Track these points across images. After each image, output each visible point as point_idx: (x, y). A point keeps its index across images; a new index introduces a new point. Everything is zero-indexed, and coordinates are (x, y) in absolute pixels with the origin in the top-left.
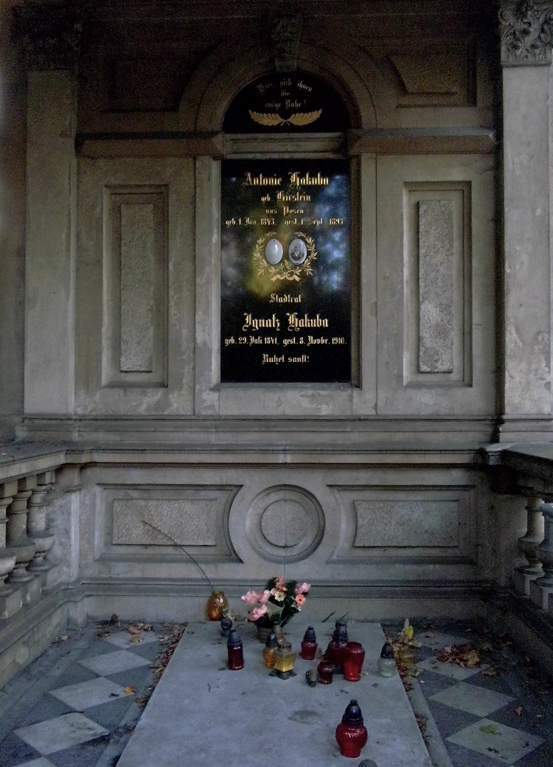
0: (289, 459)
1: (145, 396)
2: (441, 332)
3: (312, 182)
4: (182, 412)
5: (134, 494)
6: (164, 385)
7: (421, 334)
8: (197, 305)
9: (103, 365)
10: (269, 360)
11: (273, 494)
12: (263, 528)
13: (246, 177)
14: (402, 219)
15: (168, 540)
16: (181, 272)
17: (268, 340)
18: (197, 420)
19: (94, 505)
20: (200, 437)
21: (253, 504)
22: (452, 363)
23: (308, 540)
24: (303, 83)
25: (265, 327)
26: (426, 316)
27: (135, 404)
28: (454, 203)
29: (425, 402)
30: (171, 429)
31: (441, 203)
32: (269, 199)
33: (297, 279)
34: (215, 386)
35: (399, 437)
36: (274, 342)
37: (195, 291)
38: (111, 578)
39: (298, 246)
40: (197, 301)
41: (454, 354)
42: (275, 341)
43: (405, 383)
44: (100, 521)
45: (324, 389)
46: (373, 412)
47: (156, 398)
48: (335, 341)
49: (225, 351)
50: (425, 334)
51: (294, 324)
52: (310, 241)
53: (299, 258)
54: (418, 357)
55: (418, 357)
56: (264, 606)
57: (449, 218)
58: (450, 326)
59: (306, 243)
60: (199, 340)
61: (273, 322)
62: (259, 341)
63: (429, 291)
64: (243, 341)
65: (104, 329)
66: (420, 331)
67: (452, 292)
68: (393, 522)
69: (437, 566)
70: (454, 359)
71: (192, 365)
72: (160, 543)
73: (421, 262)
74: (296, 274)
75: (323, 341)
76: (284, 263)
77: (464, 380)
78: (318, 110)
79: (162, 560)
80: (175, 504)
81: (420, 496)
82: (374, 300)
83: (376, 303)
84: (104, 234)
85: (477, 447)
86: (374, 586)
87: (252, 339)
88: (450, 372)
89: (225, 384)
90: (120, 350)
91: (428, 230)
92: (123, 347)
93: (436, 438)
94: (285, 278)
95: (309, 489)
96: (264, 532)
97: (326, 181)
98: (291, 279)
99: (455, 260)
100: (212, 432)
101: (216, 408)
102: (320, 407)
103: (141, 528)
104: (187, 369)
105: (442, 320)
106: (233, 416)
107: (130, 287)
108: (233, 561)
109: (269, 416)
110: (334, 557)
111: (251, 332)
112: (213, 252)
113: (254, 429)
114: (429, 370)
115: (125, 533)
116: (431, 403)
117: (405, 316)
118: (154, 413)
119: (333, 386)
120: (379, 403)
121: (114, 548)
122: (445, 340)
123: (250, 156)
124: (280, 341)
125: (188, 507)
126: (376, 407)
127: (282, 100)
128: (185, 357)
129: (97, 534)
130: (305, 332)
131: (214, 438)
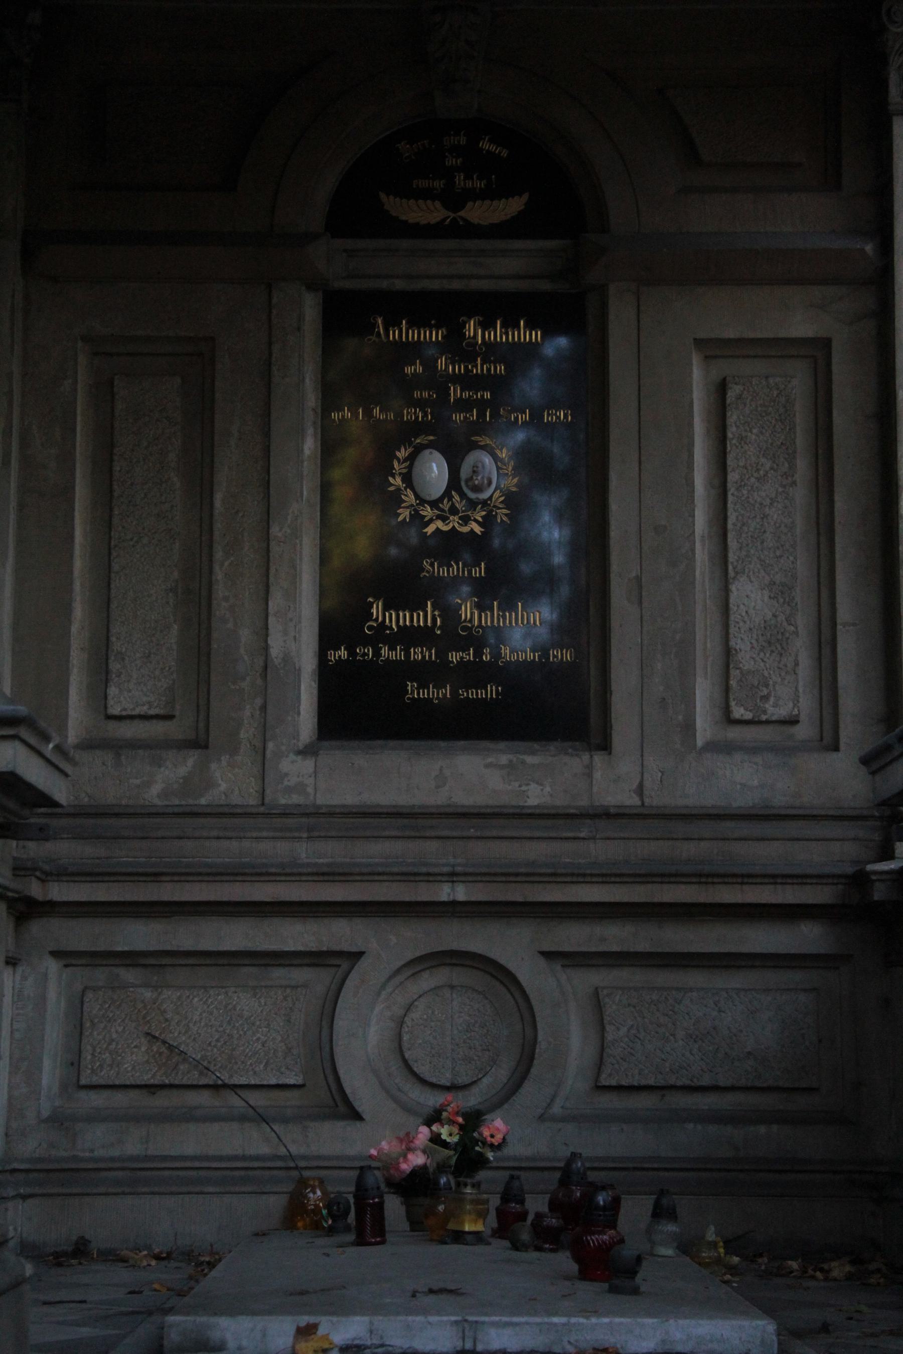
0: (461, 893)
1: (160, 767)
2: (774, 639)
3: (507, 338)
4: (235, 799)
5: (129, 975)
6: (198, 743)
7: (732, 643)
8: (271, 579)
9: (70, 702)
10: (418, 694)
11: (426, 975)
12: (405, 1045)
13: (375, 325)
14: (692, 416)
15: (201, 1073)
16: (237, 512)
17: (417, 654)
18: (267, 815)
19: (42, 998)
20: (279, 850)
21: (384, 994)
22: (796, 701)
23: (501, 1074)
24: (491, 141)
25: (412, 626)
26: (742, 606)
27: (138, 782)
28: (797, 382)
29: (742, 780)
30: (215, 833)
31: (771, 381)
32: (420, 369)
33: (478, 529)
34: (306, 747)
35: (689, 850)
36: (430, 656)
37: (268, 551)
38: (75, 1158)
39: (480, 465)
40: (272, 571)
41: (801, 684)
42: (431, 654)
43: (700, 743)
44: (54, 1035)
45: (533, 753)
46: (636, 801)
47: (182, 771)
48: (554, 656)
49: (327, 673)
50: (742, 643)
51: (471, 621)
53: (477, 489)
54: (727, 689)
55: (727, 689)
56: (419, 1153)
57: (786, 411)
58: (792, 628)
59: (496, 458)
60: (275, 651)
62: (397, 654)
63: (747, 556)
64: (365, 654)
65: (74, 629)
66: (731, 636)
67: (795, 558)
69: (775, 1128)
70: (801, 695)
71: (259, 701)
72: (185, 1081)
73: (730, 498)
74: (476, 521)
76: (451, 498)
77: (822, 740)
78: (520, 196)
79: (189, 1116)
80: (218, 995)
81: (736, 980)
83: (639, 579)
84: (78, 435)
85: (850, 870)
86: (643, 1169)
87: (385, 651)
89: (326, 744)
90: (107, 672)
91: (744, 434)
92: (114, 666)
93: (767, 853)
94: (454, 527)
95: (503, 961)
97: (536, 335)
98: (465, 529)
99: (801, 494)
100: (301, 838)
101: (310, 790)
102: (524, 788)
103: (143, 1049)
105: (775, 616)
106: (344, 806)
107: (131, 543)
108: (343, 1117)
109: (419, 807)
110: (556, 1109)
111: (381, 635)
112: (305, 473)
113: (387, 833)
114: (748, 716)
115: (109, 1061)
117: (699, 608)
118: (177, 802)
119: (552, 748)
120: (647, 784)
121: (83, 1094)
122: (781, 655)
123: (384, 284)
124: (442, 654)
125: (246, 1003)
126: (640, 790)
129: (47, 1063)
131: (305, 852)
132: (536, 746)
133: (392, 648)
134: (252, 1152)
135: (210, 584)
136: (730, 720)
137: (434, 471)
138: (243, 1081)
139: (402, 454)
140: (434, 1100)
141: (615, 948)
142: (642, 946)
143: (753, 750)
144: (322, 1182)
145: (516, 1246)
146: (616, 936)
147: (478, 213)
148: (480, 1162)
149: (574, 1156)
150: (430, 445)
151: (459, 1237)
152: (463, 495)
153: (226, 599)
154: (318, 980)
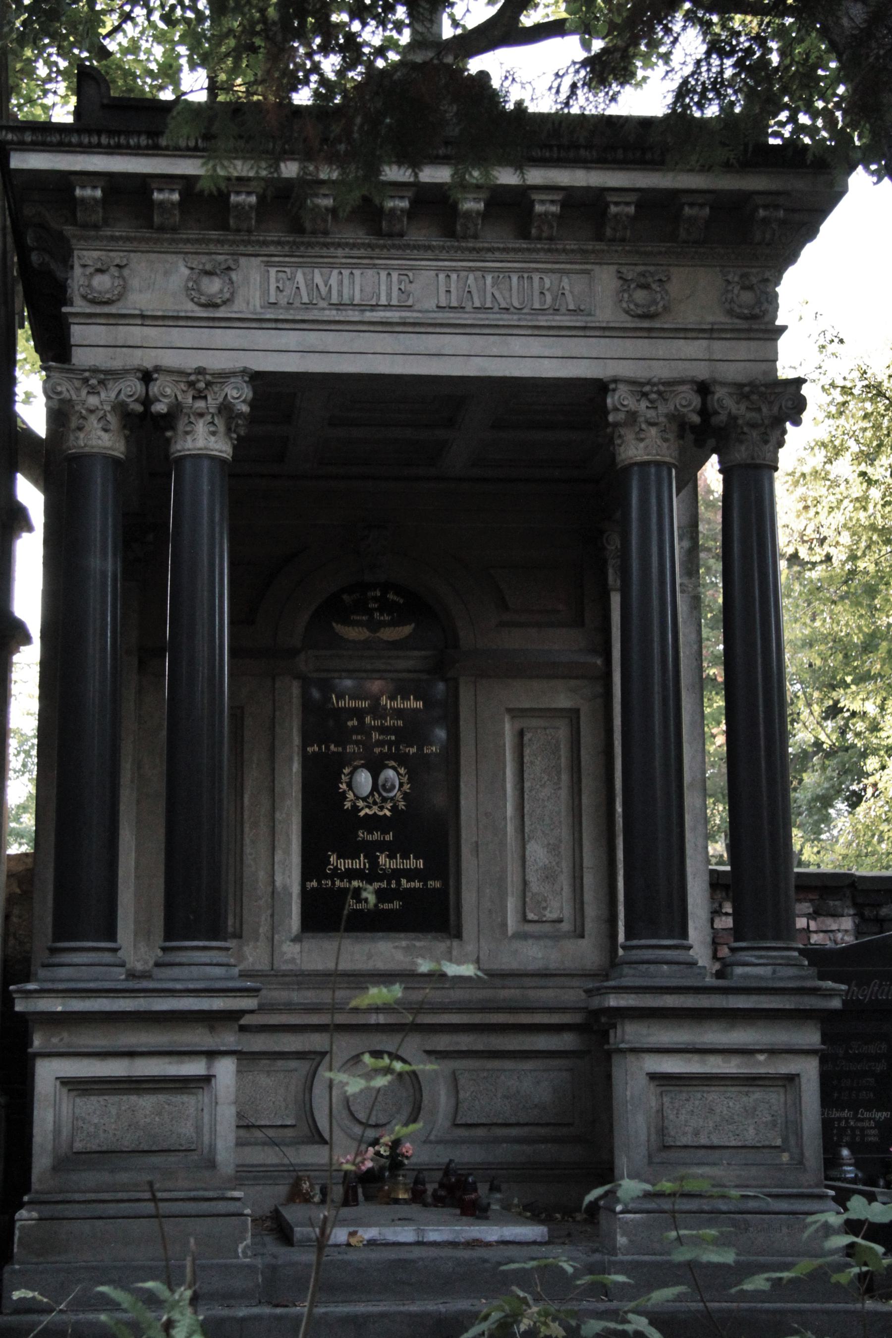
2: (549, 876)
4: (258, 967)
22: (562, 909)
28: (562, 733)
29: (533, 955)
32: (356, 723)
33: (388, 814)
43: (510, 933)
45: (420, 940)
50: (532, 877)
52: (402, 771)
55: (524, 903)
59: (398, 774)
60: (278, 884)
61: (360, 863)
68: (499, 1095)
69: (549, 1145)
71: (269, 912)
75: (417, 884)
81: (529, 1065)
82: (474, 839)
83: (477, 842)
87: (338, 883)
88: (560, 921)
89: (306, 935)
93: (547, 995)
96: (352, 1108)
98: (381, 814)
99: (564, 793)
101: (298, 961)
104: (264, 918)
108: (314, 1142)
116: (540, 955)
125: (264, 1080)
127: (370, 612)
128: (262, 902)
130: (397, 874)
131: (296, 997)
132: (420, 935)
133: (342, 881)
134: (269, 1161)
135: (242, 845)
136: (525, 920)
137: (364, 780)
138: (263, 1123)
139: (346, 771)
140: (371, 1134)
141: (464, 1048)
142: (480, 1047)
143: (538, 937)
144: (308, 1177)
145: (425, 1205)
146: (465, 1042)
147: (389, 634)
148: (401, 1164)
149: (451, 1161)
150: (363, 766)
151: (397, 1201)
152: (380, 795)
153: (251, 854)
154: (303, 1067)
